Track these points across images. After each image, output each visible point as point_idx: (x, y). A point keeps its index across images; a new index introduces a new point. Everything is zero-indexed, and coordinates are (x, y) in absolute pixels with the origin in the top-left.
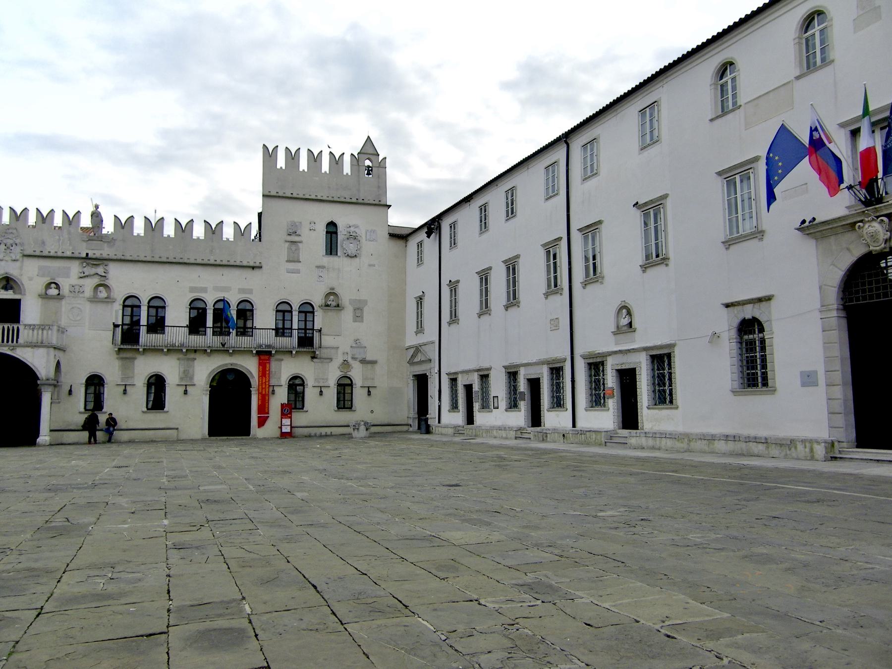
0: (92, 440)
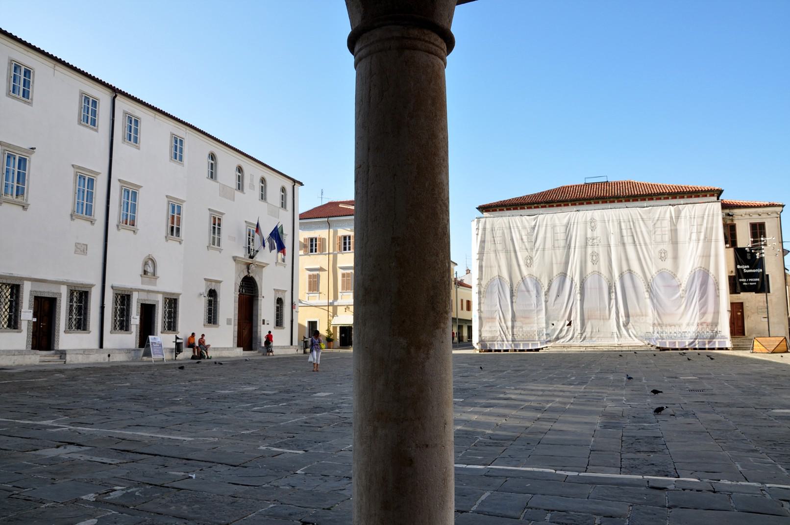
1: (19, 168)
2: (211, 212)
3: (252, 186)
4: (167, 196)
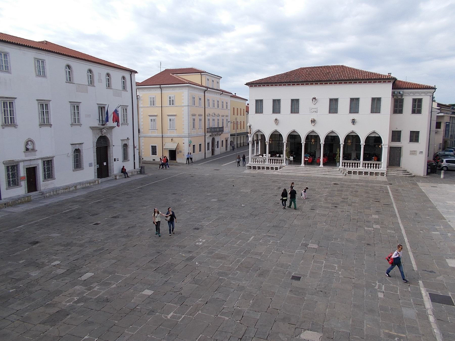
0: (126, 176)
1: (10, 108)
2: (38, 102)
3: (100, 81)
4: (97, 104)
